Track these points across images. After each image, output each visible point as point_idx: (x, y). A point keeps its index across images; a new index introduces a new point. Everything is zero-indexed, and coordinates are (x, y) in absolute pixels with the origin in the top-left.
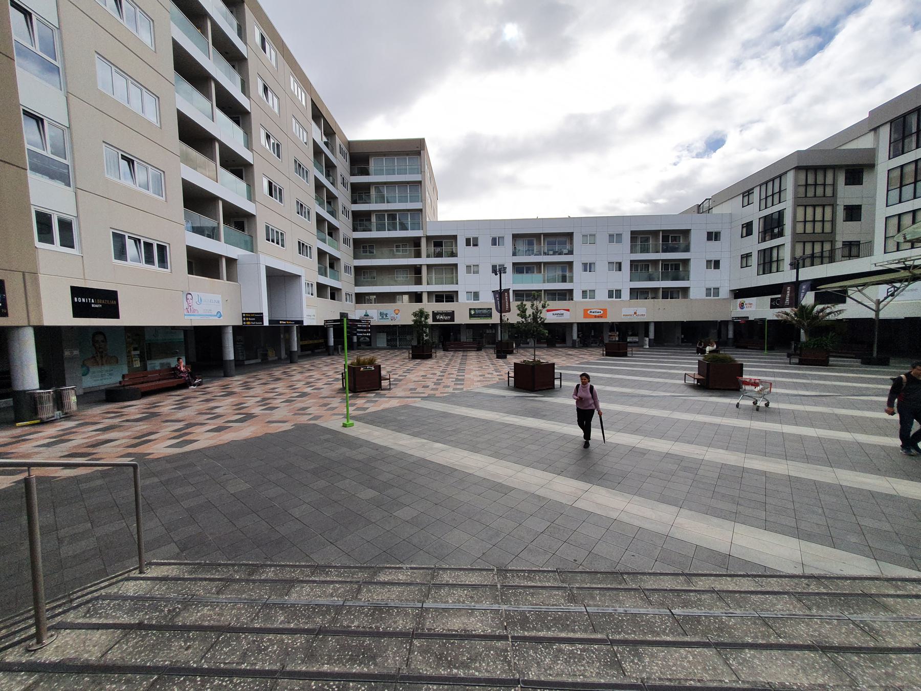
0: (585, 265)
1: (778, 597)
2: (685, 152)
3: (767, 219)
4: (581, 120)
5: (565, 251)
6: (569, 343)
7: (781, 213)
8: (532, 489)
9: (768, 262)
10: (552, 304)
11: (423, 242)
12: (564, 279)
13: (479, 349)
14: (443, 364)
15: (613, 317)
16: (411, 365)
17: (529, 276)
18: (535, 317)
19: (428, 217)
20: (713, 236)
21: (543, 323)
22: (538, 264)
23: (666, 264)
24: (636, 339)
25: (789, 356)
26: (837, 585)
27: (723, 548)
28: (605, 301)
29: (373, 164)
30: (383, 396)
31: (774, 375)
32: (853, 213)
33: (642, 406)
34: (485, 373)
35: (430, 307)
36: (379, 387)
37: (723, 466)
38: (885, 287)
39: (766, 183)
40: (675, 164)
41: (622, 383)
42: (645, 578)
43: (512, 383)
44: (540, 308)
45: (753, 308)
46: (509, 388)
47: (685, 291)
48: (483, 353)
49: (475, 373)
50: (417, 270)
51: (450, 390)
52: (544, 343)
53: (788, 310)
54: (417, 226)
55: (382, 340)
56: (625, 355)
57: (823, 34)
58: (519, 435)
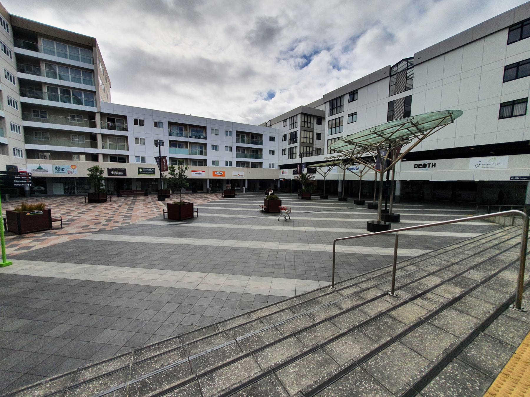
0: (213, 146)
1: (284, 312)
2: (259, 96)
3: (291, 134)
4: (208, 63)
5: (202, 137)
6: (205, 190)
7: (296, 132)
8: (170, 285)
9: (292, 154)
10: (192, 167)
11: (98, 117)
12: (201, 154)
13: (146, 195)
14: (115, 206)
15: (227, 177)
16: (87, 208)
17: (180, 149)
18: (181, 175)
19: (102, 98)
20: (272, 139)
21: (186, 179)
22: (186, 143)
23: (253, 150)
24: (239, 188)
25: (299, 195)
26: (305, 298)
27: (266, 293)
28: (224, 168)
29: (41, 43)
30: (54, 234)
31: (293, 204)
32: (319, 136)
33: (239, 224)
34: (148, 211)
35: (104, 165)
36: (50, 227)
37: (271, 250)
38: (327, 167)
39: (291, 118)
40: (255, 101)
41: (231, 212)
42: (228, 322)
43: (166, 216)
44: (184, 169)
45: (287, 174)
46: (164, 220)
47: (261, 164)
48: (149, 197)
49: (140, 211)
50: (93, 137)
51: (119, 224)
52: (190, 191)
53: (298, 175)
54: (92, 103)
55: (59, 189)
56: (233, 197)
57: (307, 59)
58: (167, 250)
